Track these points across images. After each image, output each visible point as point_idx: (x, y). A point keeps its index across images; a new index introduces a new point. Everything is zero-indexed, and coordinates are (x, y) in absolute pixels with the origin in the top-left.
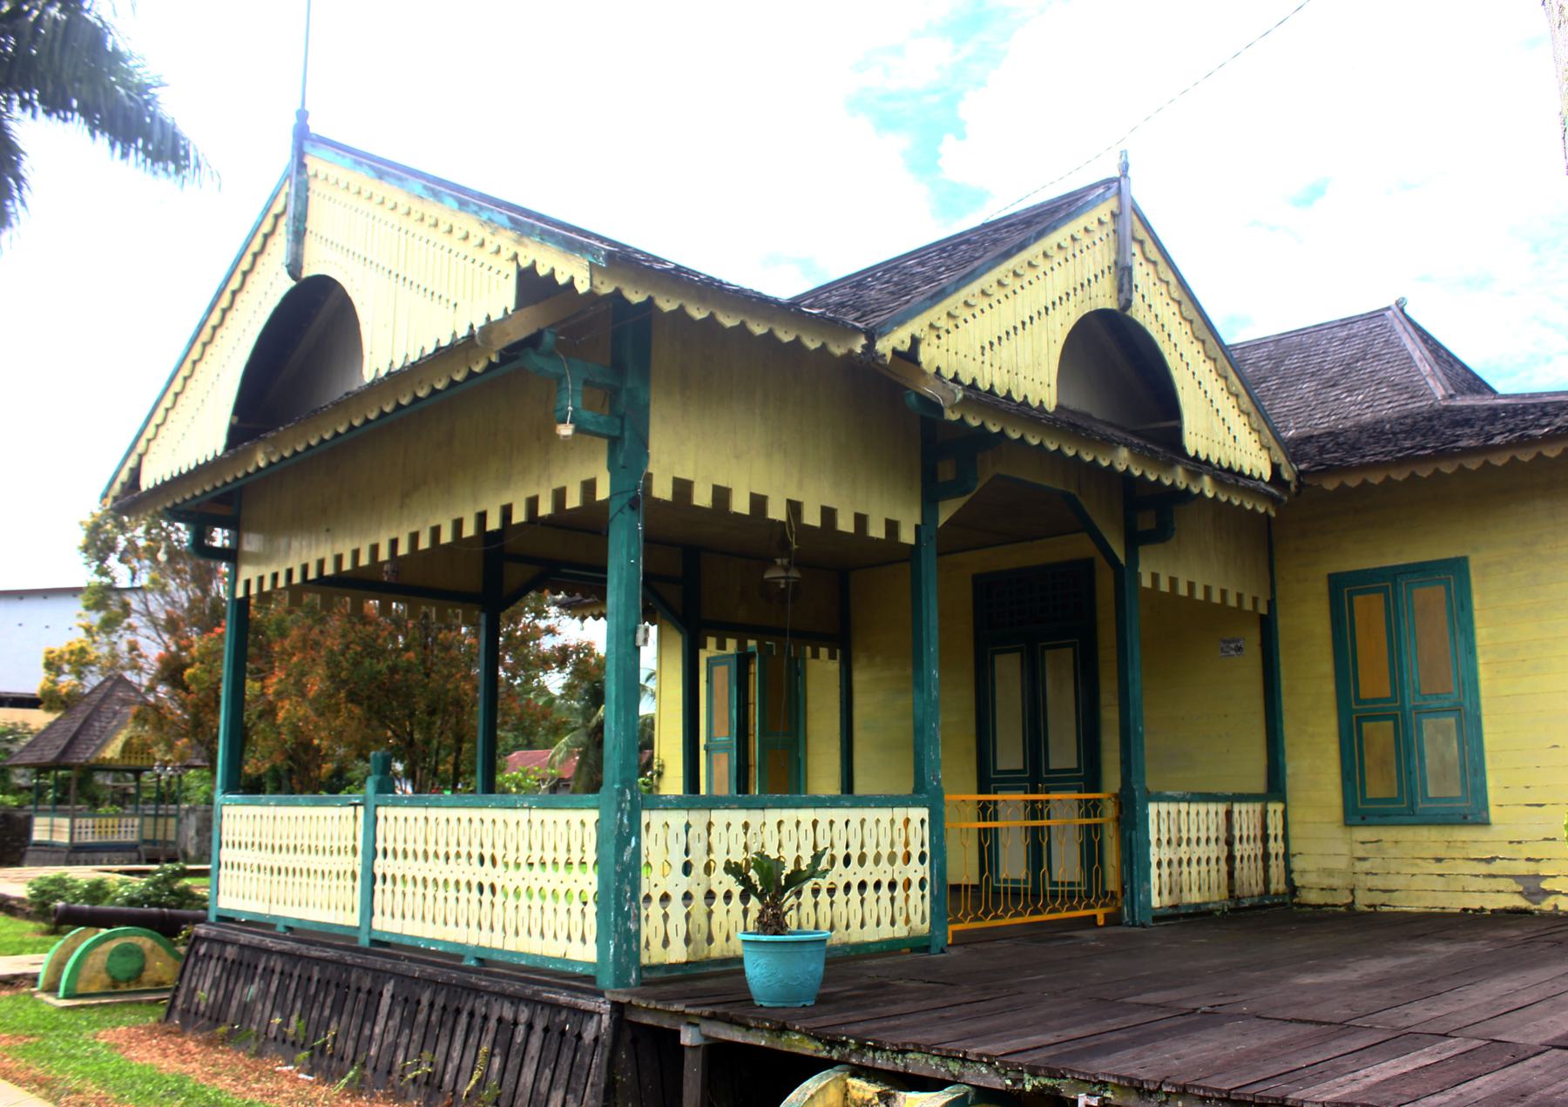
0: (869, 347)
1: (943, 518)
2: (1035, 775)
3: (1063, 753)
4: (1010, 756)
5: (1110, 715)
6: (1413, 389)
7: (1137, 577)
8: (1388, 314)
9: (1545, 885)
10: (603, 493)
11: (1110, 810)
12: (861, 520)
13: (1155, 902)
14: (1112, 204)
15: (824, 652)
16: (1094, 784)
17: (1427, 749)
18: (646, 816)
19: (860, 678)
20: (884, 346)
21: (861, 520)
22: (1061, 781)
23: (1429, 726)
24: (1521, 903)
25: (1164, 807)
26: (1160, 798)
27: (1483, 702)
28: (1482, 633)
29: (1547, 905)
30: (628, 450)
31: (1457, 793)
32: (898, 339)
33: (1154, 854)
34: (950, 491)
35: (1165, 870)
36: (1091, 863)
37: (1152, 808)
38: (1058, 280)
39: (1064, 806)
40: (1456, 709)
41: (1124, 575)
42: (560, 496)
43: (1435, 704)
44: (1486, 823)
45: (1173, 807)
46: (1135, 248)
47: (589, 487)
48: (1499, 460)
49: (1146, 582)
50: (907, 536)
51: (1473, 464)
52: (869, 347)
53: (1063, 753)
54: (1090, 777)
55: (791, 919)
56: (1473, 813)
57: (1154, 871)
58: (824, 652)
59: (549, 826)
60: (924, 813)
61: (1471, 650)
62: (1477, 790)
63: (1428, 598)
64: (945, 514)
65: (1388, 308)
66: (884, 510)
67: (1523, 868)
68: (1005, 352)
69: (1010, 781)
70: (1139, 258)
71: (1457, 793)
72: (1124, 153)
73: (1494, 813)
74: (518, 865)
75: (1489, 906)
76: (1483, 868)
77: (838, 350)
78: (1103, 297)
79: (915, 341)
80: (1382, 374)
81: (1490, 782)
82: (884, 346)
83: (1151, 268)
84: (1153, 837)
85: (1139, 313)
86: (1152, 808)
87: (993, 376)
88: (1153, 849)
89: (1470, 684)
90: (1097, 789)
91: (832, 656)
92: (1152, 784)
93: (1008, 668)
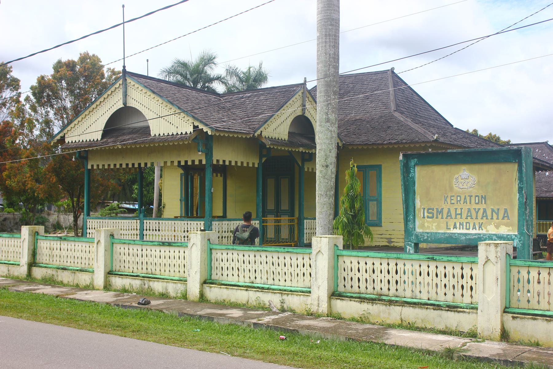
0: (254, 135)
1: (263, 161)
2: (277, 212)
3: (285, 206)
4: (271, 206)
5: (297, 197)
6: (386, 105)
7: (304, 168)
8: (388, 72)
9: (392, 240)
10: (204, 162)
11: (296, 221)
12: (248, 163)
13: (305, 242)
14: (302, 91)
15: (219, 175)
16: (293, 215)
17: (370, 209)
18: (213, 222)
19: (229, 182)
20: (256, 134)
21: (248, 163)
22: (284, 213)
23: (371, 203)
24: (387, 244)
25: (308, 221)
26: (307, 219)
27: (383, 199)
28: (384, 183)
29: (392, 245)
30: (209, 154)
31: (376, 219)
32: (258, 132)
33: (305, 231)
34: (265, 156)
35: (308, 235)
36: (291, 233)
37: (305, 221)
38: (290, 110)
39: (285, 220)
40: (377, 200)
41: (301, 168)
42: (193, 161)
43: (372, 199)
44: (381, 226)
45: (310, 221)
46: (307, 99)
47: (200, 161)
48: (385, 147)
49: (306, 170)
50: (256, 166)
51: (380, 147)
52: (254, 135)
53: (285, 206)
54: (291, 213)
55: (456, 188)
56: (378, 224)
57: (305, 235)
58: (219, 175)
59: (192, 224)
60: (258, 222)
61: (381, 187)
62: (380, 219)
63: (372, 173)
64: (264, 160)
65: (388, 70)
66: (253, 161)
67: (388, 236)
68: (278, 130)
69: (271, 212)
70: (307, 101)
71: (376, 219)
72: (305, 78)
73: (383, 224)
74: (156, 230)
75: (381, 245)
76: (380, 236)
77: (248, 137)
78: (299, 113)
79: (261, 132)
80: (381, 98)
81: (383, 217)
82: (256, 134)
83: (310, 103)
84: (305, 227)
85: (307, 114)
86: (305, 221)
87: (275, 135)
88: (305, 230)
89: (380, 194)
90: (293, 217)
91: (221, 176)
92: (305, 215)
93: (271, 183)
